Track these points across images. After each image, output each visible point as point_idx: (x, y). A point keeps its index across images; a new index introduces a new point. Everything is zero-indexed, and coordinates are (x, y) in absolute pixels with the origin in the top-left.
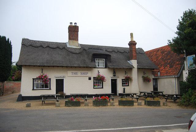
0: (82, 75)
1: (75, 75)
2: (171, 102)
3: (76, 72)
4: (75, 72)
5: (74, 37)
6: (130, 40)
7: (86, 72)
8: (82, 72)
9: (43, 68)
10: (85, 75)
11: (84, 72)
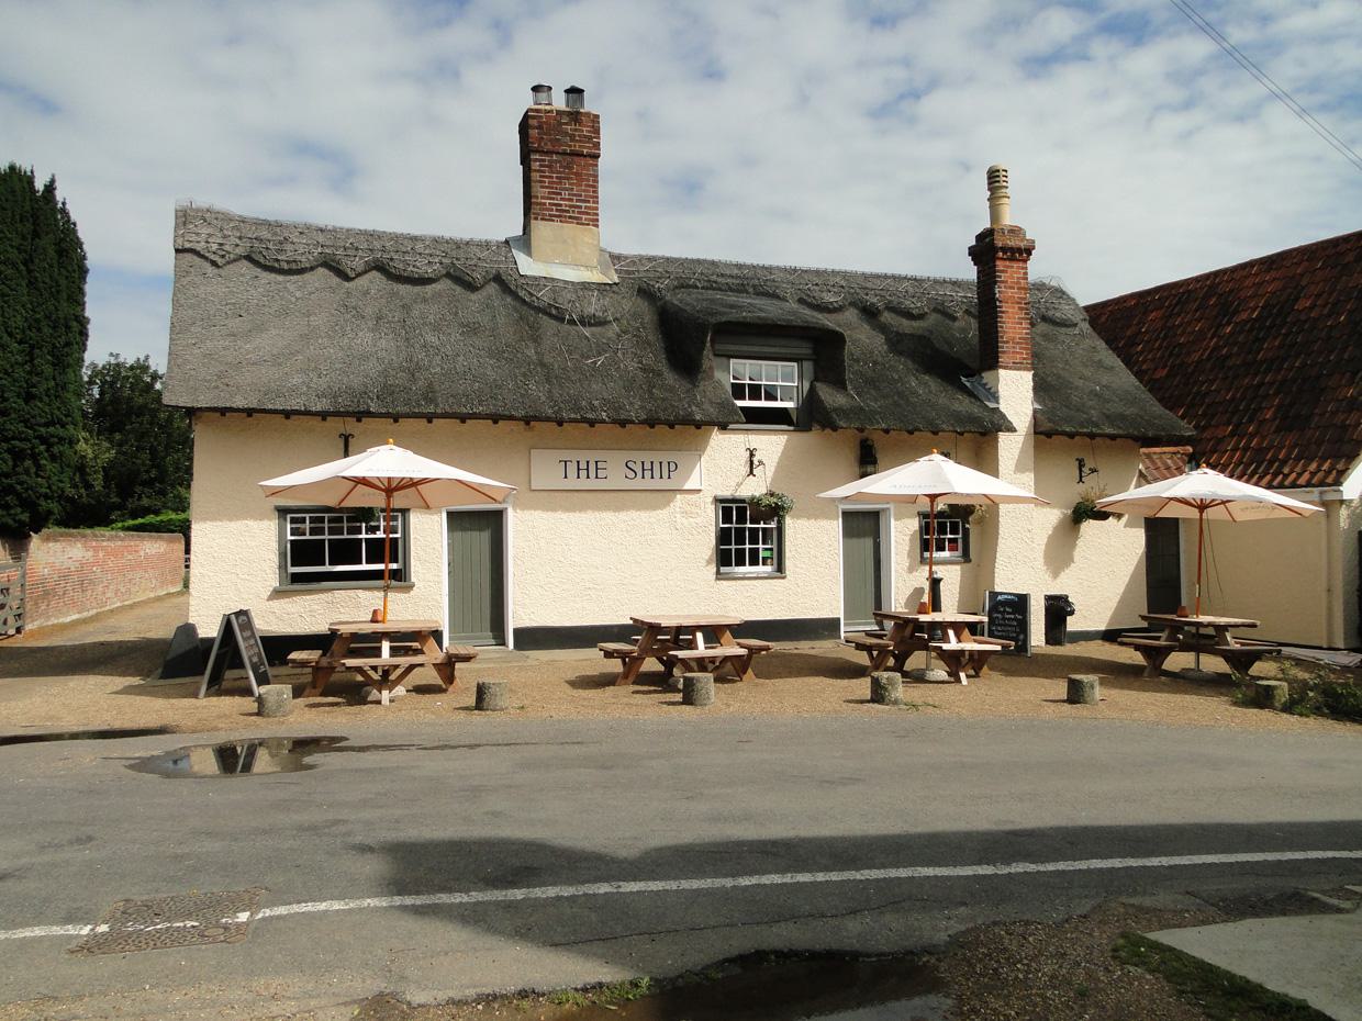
0: (638, 483)
1: (584, 483)
2: (1262, 678)
3: (592, 456)
4: (584, 456)
5: (566, 194)
6: (989, 226)
7: (665, 457)
8: (639, 456)
9: (351, 426)
10: (657, 484)
11: (647, 457)
